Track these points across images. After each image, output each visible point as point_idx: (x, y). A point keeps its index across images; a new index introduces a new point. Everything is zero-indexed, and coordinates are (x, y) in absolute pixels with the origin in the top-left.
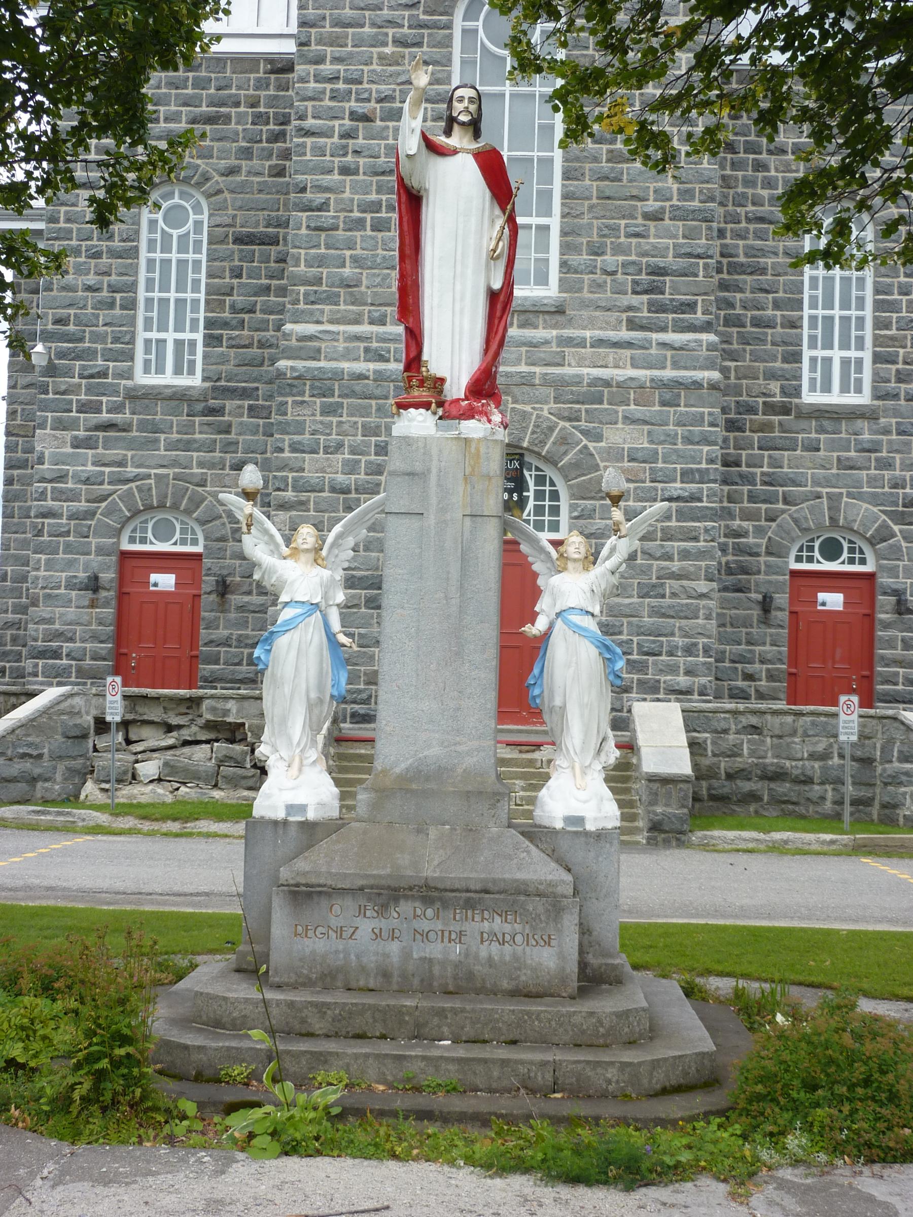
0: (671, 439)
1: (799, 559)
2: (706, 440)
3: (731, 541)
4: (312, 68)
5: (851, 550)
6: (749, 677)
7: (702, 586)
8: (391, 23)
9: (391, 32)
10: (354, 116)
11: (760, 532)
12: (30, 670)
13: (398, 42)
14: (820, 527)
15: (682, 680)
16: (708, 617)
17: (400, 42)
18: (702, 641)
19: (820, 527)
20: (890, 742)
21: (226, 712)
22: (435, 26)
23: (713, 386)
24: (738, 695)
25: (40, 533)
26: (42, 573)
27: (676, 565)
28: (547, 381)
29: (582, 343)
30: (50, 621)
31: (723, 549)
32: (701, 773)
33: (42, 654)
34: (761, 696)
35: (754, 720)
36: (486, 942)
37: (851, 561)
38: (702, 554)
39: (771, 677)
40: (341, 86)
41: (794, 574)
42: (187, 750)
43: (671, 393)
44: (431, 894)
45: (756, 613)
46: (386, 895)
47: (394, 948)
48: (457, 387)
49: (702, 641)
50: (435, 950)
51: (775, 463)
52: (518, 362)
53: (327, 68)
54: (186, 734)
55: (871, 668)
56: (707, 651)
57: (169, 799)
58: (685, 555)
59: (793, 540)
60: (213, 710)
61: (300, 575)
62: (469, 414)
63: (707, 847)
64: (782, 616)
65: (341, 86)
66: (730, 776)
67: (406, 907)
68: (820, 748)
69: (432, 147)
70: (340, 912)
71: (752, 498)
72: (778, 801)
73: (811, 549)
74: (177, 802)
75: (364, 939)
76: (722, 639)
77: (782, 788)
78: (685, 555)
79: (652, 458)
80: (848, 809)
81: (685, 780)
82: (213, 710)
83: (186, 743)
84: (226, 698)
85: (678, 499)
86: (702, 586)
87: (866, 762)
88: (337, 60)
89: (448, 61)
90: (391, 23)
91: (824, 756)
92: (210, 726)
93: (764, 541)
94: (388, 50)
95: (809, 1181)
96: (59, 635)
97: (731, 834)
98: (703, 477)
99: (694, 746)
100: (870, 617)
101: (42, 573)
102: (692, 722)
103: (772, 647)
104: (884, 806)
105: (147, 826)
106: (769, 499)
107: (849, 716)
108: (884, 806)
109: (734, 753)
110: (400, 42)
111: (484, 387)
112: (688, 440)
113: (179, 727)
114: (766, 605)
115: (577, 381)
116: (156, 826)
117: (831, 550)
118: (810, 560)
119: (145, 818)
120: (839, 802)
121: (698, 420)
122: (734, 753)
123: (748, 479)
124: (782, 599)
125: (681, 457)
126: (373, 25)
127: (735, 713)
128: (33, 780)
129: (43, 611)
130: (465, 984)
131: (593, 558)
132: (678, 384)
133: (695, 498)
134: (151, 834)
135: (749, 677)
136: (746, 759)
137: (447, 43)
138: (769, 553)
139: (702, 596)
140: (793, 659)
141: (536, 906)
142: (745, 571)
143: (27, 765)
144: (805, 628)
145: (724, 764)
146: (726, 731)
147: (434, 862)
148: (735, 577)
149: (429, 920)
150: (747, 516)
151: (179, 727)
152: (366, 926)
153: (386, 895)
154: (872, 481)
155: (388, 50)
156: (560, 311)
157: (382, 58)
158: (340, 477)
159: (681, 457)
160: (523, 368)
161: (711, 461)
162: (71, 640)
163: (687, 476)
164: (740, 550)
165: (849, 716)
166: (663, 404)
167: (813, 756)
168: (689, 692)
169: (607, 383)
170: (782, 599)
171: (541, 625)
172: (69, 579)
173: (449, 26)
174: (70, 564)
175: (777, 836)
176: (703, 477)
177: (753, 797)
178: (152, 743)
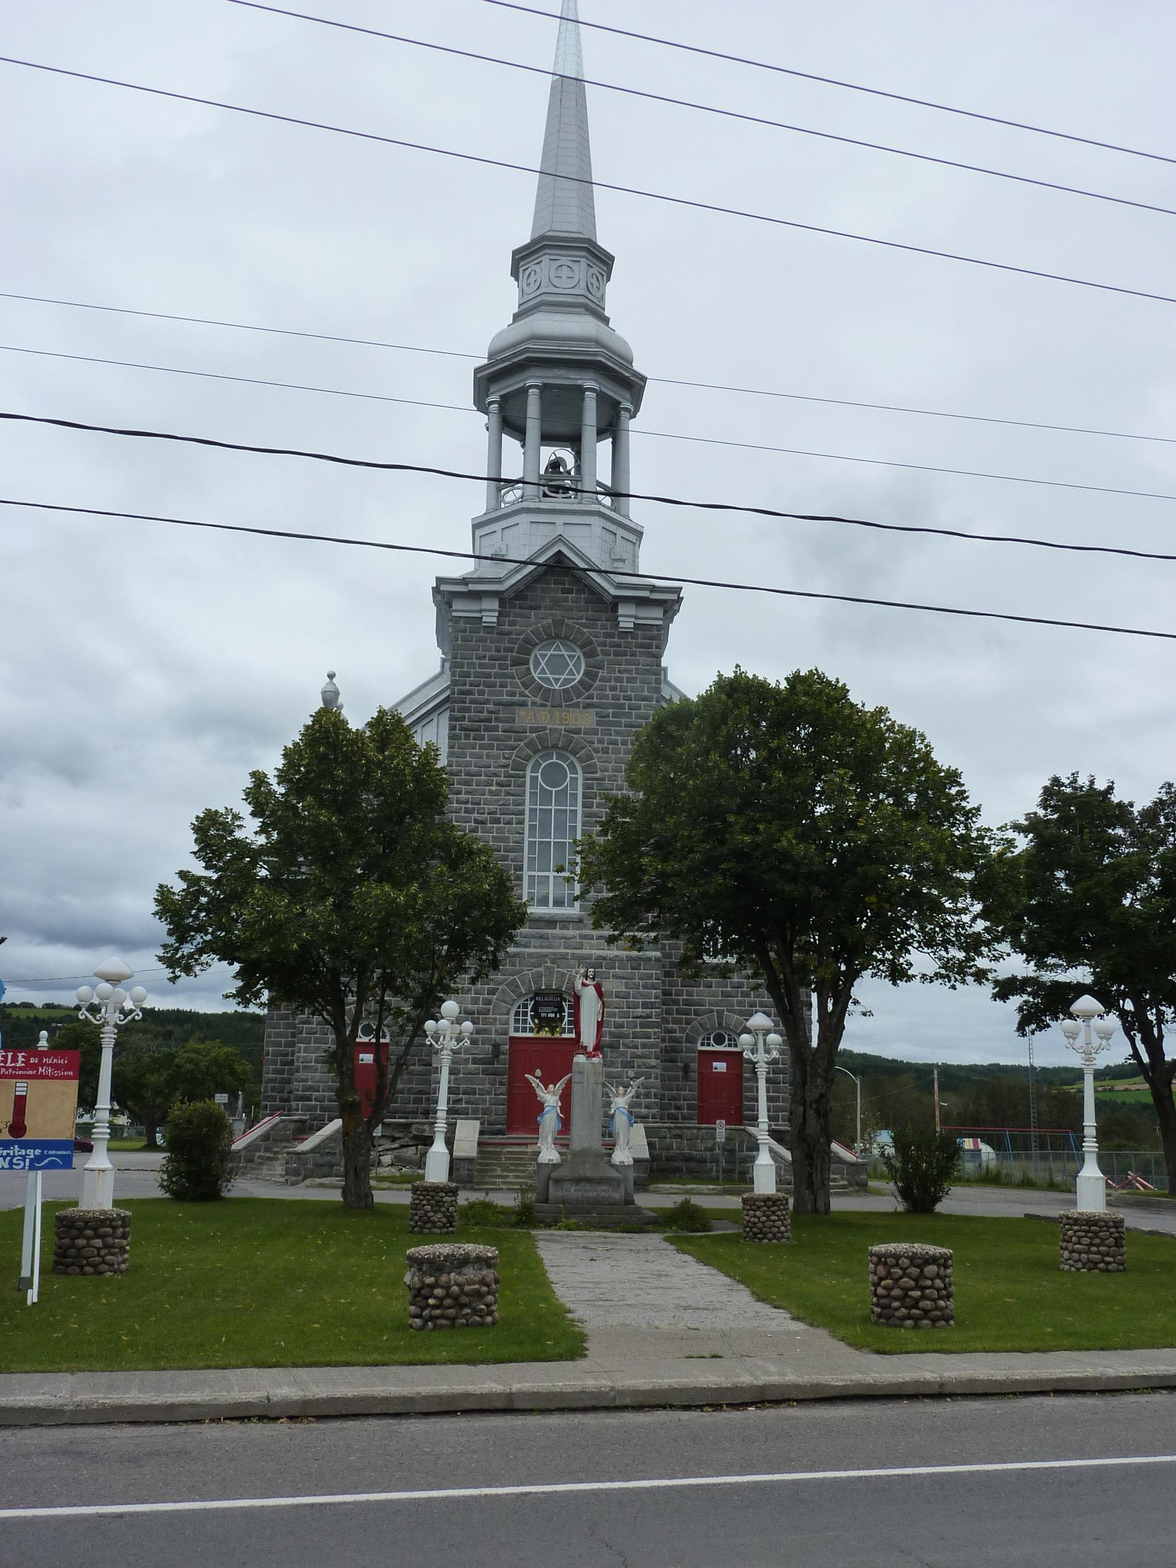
0: (637, 986)
1: (703, 1044)
2: (654, 987)
3: (667, 1035)
4: (455, 797)
5: (730, 1040)
6: (678, 1108)
7: (653, 1062)
8: (495, 775)
9: (495, 779)
10: (476, 821)
11: (682, 1030)
12: (294, 1107)
13: (498, 784)
14: (713, 1028)
15: (644, 1111)
16: (656, 1078)
17: (499, 784)
18: (653, 1090)
19: (713, 1028)
20: (742, 1143)
21: (424, 1131)
22: (517, 776)
23: (657, 960)
24: (673, 1118)
25: (301, 1032)
26: (302, 1054)
27: (640, 1051)
28: (574, 957)
29: (591, 938)
30: (306, 1081)
31: (663, 1040)
32: (654, 1157)
33: (302, 1099)
34: (684, 1118)
35: (678, 1132)
36: (603, 1192)
37: (730, 1045)
38: (653, 1046)
39: (689, 1108)
40: (470, 806)
41: (701, 1052)
42: (404, 1150)
43: (636, 963)
44: (589, 1180)
45: (680, 1073)
46: (578, 1181)
47: (580, 1194)
48: (590, 1049)
49: (653, 1090)
50: (590, 1194)
51: (689, 994)
52: (559, 947)
53: (463, 796)
54: (402, 1142)
55: (741, 1102)
56: (656, 1096)
57: (398, 1174)
58: (644, 1046)
59: (699, 1035)
60: (417, 1129)
61: (550, 1098)
62: (594, 1056)
63: (656, 1192)
64: (695, 1075)
65: (470, 806)
66: (667, 1159)
67: (582, 1184)
68: (710, 1145)
69: (584, 985)
70: (566, 1185)
71: (678, 1012)
72: (690, 1171)
73: (709, 1039)
74: (402, 1176)
75: (572, 1192)
76: (663, 1088)
77: (692, 1165)
78: (644, 1046)
79: (627, 996)
80: (721, 1175)
81: (645, 1160)
82: (417, 1129)
83: (403, 1146)
84: (424, 1124)
85: (641, 1017)
86: (653, 1062)
87: (732, 1152)
88: (468, 793)
89: (524, 794)
90: (495, 775)
91: (712, 1149)
92: (415, 1138)
93: (684, 1036)
94: (494, 788)
95: (613, 952)
96: (310, 1088)
97: (667, 1186)
98: (653, 1006)
99: (650, 1144)
100: (740, 1075)
101: (302, 1054)
102: (649, 1133)
103: (690, 1091)
104: (740, 1173)
105: (395, 1186)
106: (687, 1013)
107: (721, 1130)
108: (740, 1173)
109: (669, 1148)
110: (499, 784)
111: (598, 1047)
112: (645, 987)
113: (399, 1138)
114: (686, 1069)
115: (589, 957)
116: (399, 1186)
117: (719, 1040)
118: (709, 1045)
119: (394, 1182)
120: (718, 1172)
121: (650, 977)
122: (669, 1148)
123: (676, 1002)
124: (694, 1066)
125: (642, 996)
126: (486, 775)
127: (669, 1128)
128: (331, 1165)
129: (302, 1075)
130: (597, 1202)
131: (624, 1095)
132: (640, 959)
133: (649, 1016)
134: (398, 1189)
135: (678, 1108)
136: (675, 1151)
137: (523, 785)
138: (687, 1042)
139: (653, 1067)
140: (701, 1098)
141: (614, 1183)
142: (674, 1050)
143: (329, 1158)
144: (707, 1079)
145: (664, 1153)
146: (665, 1137)
147: (589, 1172)
148: (669, 1055)
149: (588, 1187)
150: (675, 1022)
151: (399, 1138)
152: (573, 1189)
153: (578, 1181)
154: (740, 1003)
155: (494, 788)
156: (580, 921)
157: (490, 792)
158: (469, 1006)
159: (642, 996)
160: (562, 950)
161: (656, 998)
162: (318, 1091)
163: (645, 1006)
164: (671, 1040)
165: (721, 1130)
166: (632, 968)
167: (707, 1149)
168: (646, 1117)
169: (604, 958)
170: (694, 1066)
171: (612, 1111)
172: (316, 1058)
173: (524, 776)
174: (317, 1049)
175: (689, 1187)
176: (653, 1006)
177: (679, 1170)
178: (387, 1147)
